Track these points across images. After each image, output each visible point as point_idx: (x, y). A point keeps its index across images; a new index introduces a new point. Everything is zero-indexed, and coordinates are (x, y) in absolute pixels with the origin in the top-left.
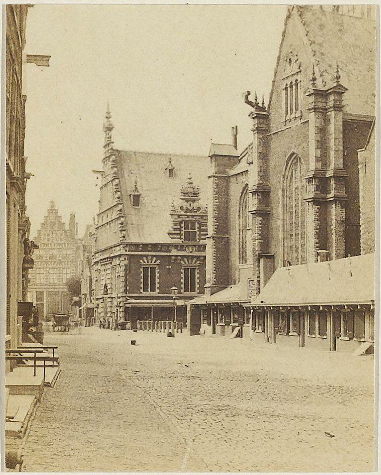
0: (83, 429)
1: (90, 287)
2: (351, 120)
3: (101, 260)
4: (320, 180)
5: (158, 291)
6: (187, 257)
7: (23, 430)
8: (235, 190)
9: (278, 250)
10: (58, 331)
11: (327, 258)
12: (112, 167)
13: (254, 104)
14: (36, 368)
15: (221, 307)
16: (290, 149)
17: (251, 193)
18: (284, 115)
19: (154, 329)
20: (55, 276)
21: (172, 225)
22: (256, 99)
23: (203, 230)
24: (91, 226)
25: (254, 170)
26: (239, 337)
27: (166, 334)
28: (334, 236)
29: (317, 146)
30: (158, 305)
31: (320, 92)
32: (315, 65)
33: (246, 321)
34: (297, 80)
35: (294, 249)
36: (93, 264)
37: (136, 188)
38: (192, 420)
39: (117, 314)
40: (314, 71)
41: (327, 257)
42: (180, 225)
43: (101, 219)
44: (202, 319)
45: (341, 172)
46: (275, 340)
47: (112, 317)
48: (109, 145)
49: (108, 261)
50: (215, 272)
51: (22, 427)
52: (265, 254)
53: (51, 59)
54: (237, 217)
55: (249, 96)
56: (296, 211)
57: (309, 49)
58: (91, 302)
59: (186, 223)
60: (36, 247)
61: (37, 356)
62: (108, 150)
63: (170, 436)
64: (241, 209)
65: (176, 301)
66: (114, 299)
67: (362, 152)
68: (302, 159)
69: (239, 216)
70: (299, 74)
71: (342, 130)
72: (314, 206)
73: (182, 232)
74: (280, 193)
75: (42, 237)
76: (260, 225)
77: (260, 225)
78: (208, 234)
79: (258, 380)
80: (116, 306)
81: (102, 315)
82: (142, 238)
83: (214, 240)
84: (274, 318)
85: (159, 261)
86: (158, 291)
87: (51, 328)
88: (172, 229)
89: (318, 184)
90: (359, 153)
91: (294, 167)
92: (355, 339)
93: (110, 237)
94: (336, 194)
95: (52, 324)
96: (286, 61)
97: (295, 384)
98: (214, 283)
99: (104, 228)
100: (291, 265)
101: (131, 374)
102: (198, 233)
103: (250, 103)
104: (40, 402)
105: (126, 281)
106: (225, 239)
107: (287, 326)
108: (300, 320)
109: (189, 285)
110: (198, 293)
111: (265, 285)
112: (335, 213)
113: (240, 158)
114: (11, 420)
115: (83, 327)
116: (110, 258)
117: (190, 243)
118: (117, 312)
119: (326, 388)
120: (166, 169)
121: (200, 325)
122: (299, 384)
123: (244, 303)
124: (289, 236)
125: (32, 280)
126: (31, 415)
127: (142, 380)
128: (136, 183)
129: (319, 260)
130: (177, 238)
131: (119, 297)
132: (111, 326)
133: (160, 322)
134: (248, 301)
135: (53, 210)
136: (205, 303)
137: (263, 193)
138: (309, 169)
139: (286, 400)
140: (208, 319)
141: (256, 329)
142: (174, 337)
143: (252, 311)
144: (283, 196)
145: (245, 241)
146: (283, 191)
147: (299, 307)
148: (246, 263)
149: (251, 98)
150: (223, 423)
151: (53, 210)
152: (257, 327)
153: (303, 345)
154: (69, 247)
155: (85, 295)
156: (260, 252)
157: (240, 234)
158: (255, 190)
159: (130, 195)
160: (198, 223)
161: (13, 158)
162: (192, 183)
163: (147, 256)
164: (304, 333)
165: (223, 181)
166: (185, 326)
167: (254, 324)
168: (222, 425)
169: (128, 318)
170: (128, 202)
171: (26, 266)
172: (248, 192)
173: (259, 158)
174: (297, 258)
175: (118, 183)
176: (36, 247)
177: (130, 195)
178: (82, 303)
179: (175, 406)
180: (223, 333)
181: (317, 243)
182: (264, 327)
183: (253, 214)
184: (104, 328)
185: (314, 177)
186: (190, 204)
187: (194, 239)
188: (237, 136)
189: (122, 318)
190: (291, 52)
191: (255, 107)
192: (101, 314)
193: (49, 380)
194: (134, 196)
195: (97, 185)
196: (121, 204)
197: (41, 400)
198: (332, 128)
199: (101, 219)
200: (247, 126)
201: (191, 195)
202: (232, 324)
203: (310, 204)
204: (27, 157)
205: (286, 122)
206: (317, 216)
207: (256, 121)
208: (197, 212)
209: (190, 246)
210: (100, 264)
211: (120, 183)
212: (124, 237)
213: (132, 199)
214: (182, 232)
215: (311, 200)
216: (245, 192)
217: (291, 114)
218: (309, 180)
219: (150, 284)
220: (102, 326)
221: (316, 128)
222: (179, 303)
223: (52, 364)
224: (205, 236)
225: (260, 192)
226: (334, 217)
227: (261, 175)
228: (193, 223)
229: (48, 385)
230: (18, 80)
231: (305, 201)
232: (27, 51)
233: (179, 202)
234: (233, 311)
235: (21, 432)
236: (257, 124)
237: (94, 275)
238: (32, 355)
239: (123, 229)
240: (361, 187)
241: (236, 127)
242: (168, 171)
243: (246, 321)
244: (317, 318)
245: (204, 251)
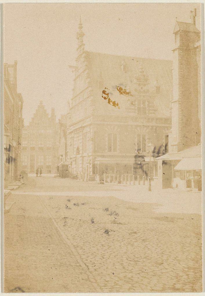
1: (66, 149)
58: (66, 160)
241: (195, 9)
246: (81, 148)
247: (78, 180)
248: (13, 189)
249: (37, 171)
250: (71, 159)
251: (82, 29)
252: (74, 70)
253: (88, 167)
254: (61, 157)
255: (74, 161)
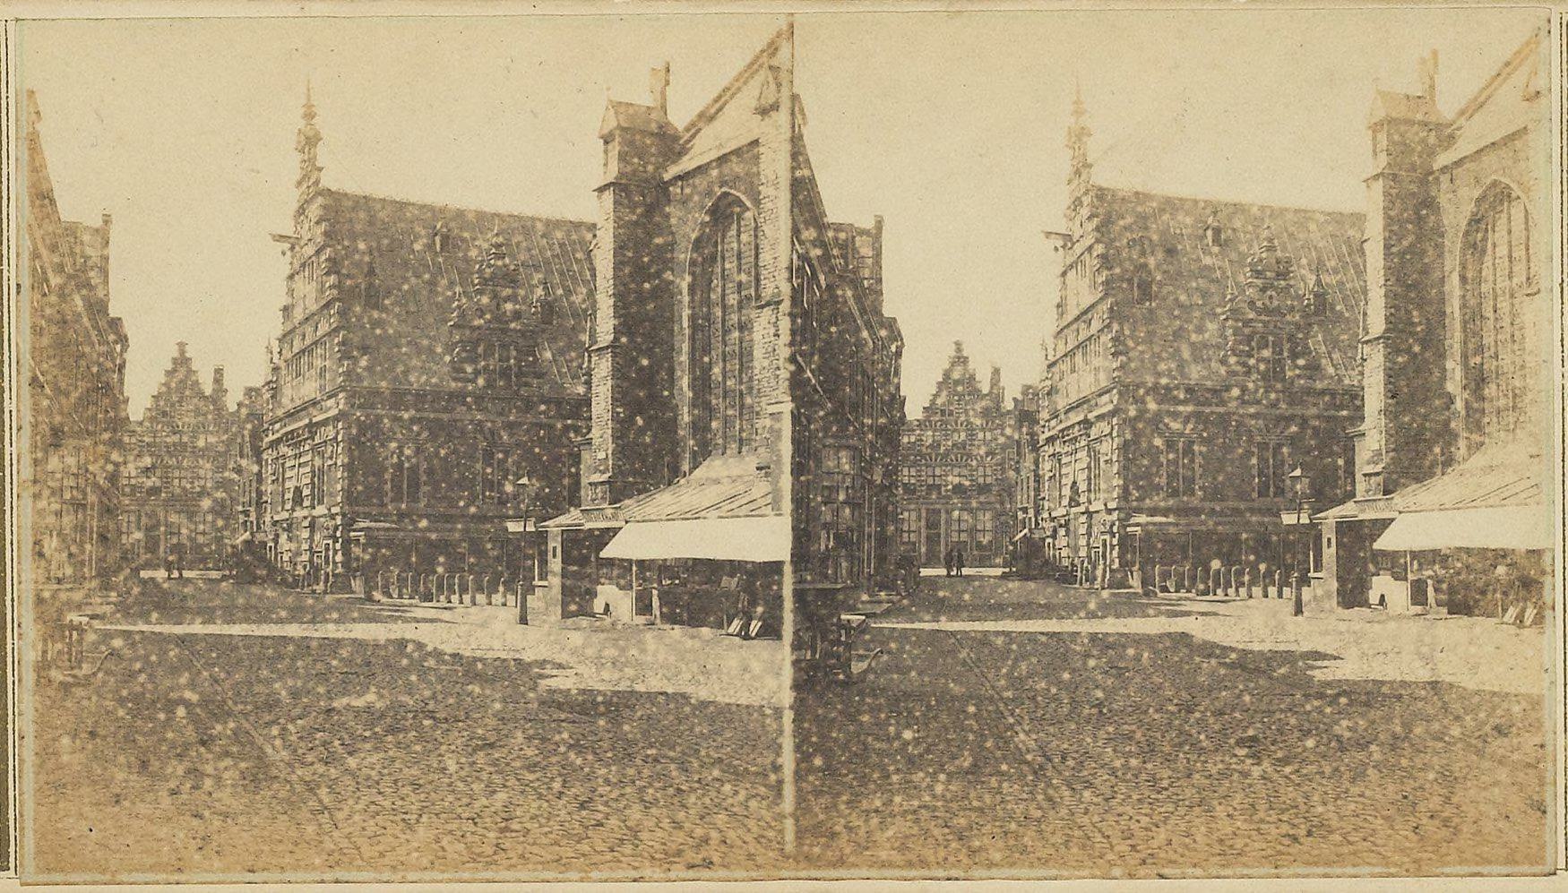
58: (1037, 524)
246: (1083, 487)
247: (1077, 586)
248: (874, 615)
249: (949, 555)
250: (1053, 519)
251: (313, 121)
252: (287, 246)
253: (1105, 545)
254: (1020, 515)
255: (1061, 526)
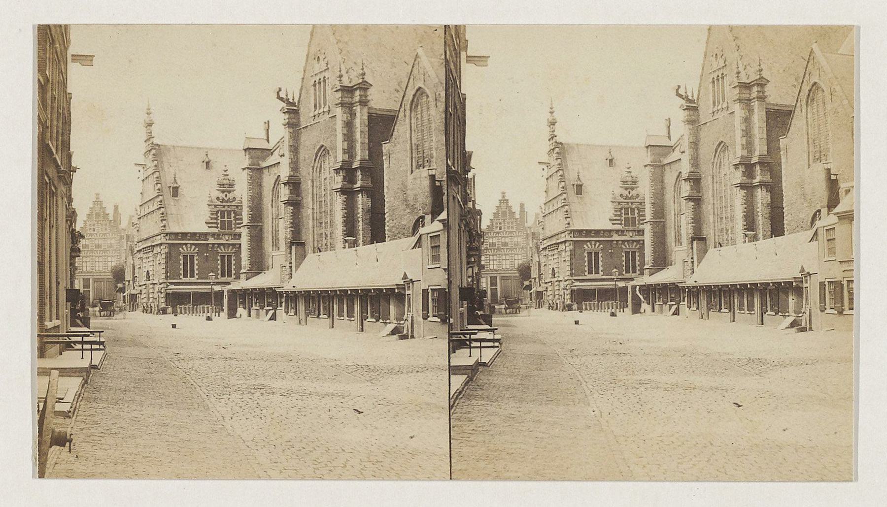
0: (128, 409)
2: (376, 114)
3: (143, 248)
4: (347, 170)
5: (601, 273)
6: (628, 241)
7: (72, 410)
8: (268, 181)
9: (308, 236)
10: (104, 316)
11: (354, 245)
12: (153, 161)
13: (684, 97)
14: (93, 352)
15: (255, 292)
16: (718, 139)
17: (283, 183)
18: (712, 107)
19: (598, 309)
20: (101, 264)
21: (210, 215)
22: (287, 95)
23: (238, 219)
24: (133, 216)
25: (285, 162)
26: (676, 314)
27: (205, 318)
28: (360, 223)
29: (344, 139)
30: (602, 287)
31: (744, 85)
32: (341, 63)
33: (279, 305)
34: (723, 74)
35: (324, 236)
36: (136, 252)
37: (579, 178)
38: (229, 398)
39: (159, 300)
40: (738, 65)
41: (355, 244)
42: (217, 215)
43: (143, 210)
44: (238, 303)
45: (765, 159)
46: (306, 323)
47: (154, 302)
48: (552, 138)
49: (149, 249)
50: (250, 258)
51: (71, 407)
52: (698, 237)
53: (94, 58)
54: (672, 204)
55: (280, 93)
56: (325, 201)
57: (733, 44)
59: (223, 213)
60: (83, 237)
61: (84, 340)
62: (149, 145)
63: (209, 414)
64: (274, 199)
65: (213, 286)
66: (155, 285)
67: (784, 139)
68: (330, 152)
69: (272, 205)
70: (725, 68)
71: (367, 123)
72: (341, 196)
73: (219, 221)
74: (310, 183)
75: (88, 227)
76: (292, 214)
77: (292, 214)
78: (242, 223)
79: (291, 361)
80: (564, 289)
81: (145, 300)
82: (182, 228)
83: (651, 224)
84: (305, 302)
85: (197, 249)
86: (197, 277)
87: (98, 314)
88: (209, 219)
89: (345, 175)
90: (383, 145)
91: (323, 158)
92: (381, 321)
93: (151, 227)
94: (363, 184)
95: (98, 310)
96: (315, 59)
97: (325, 364)
98: (249, 269)
99: (550, 216)
100: (320, 251)
101: (172, 356)
102: (234, 222)
103: (281, 99)
104: (87, 383)
105: (571, 265)
106: (259, 228)
107: (317, 310)
108: (329, 304)
109: (226, 271)
110: (234, 279)
111: (296, 270)
112: (362, 202)
113: (272, 151)
114: (60, 401)
115: (127, 312)
116: (152, 246)
117: (227, 231)
118: (564, 294)
119: (746, 360)
120: (203, 162)
121: (641, 305)
122: (329, 364)
123: (277, 288)
124: (318, 224)
125: (79, 268)
126: (79, 395)
127: (183, 361)
128: (578, 173)
129: (747, 241)
130: (215, 227)
131: (161, 283)
132: (153, 311)
133: (198, 306)
134: (683, 281)
135: (98, 202)
136: (644, 284)
137: (294, 184)
138: (337, 160)
139: (317, 379)
140: (243, 303)
141: (691, 307)
142: (616, 316)
143: (285, 295)
144: (713, 182)
145: (277, 229)
146: (713, 177)
147: (328, 291)
148: (681, 245)
149: (282, 95)
150: (258, 401)
151: (98, 202)
152: (289, 311)
153: (333, 327)
154: (113, 236)
155: (129, 281)
156: (694, 235)
157: (272, 223)
158: (687, 178)
159: (573, 185)
160: (638, 209)
161: (60, 152)
162: (630, 172)
163: (186, 244)
164: (333, 316)
165: (256, 172)
166: (223, 310)
167: (287, 307)
168: (258, 404)
169: (169, 304)
170: (168, 194)
171: (73, 255)
172: (280, 183)
173: (290, 151)
174: (727, 239)
175: (159, 176)
176: (83, 237)
177: (573, 185)
178: (126, 290)
179: (214, 386)
180: (258, 315)
181: (345, 231)
182: (698, 305)
183: (686, 199)
184: (552, 309)
185: (341, 168)
186: (629, 192)
187: (230, 228)
188: (269, 130)
189: (163, 303)
190: (319, 51)
191: (286, 102)
192: (550, 296)
193: (485, 360)
194: (173, 188)
195: (543, 176)
196: (161, 195)
197: (89, 381)
198: (357, 122)
199: (143, 210)
200: (679, 115)
201: (227, 187)
202: (669, 303)
203: (338, 194)
204: (73, 152)
205: (314, 116)
206: (745, 200)
207: (287, 116)
208: (232, 202)
209: (226, 234)
210: (142, 252)
211: (564, 174)
212: (164, 226)
213: (171, 190)
214: (219, 221)
215: (338, 190)
216: (277, 183)
217: (320, 109)
218: (337, 171)
219: (593, 267)
220: (145, 310)
221: (343, 122)
222: (217, 288)
223: (493, 345)
224: (239, 224)
225: (691, 179)
226: (360, 206)
227: (292, 166)
228: (229, 213)
229: (94, 367)
230: (64, 80)
231: (333, 191)
232: (72, 51)
233: (619, 191)
234: (670, 291)
235: (70, 412)
236: (288, 119)
237: (137, 262)
238: (80, 339)
239: (164, 218)
240: (386, 178)
242: (608, 160)
243: (279, 305)
244: (745, 296)
245: (239, 239)
